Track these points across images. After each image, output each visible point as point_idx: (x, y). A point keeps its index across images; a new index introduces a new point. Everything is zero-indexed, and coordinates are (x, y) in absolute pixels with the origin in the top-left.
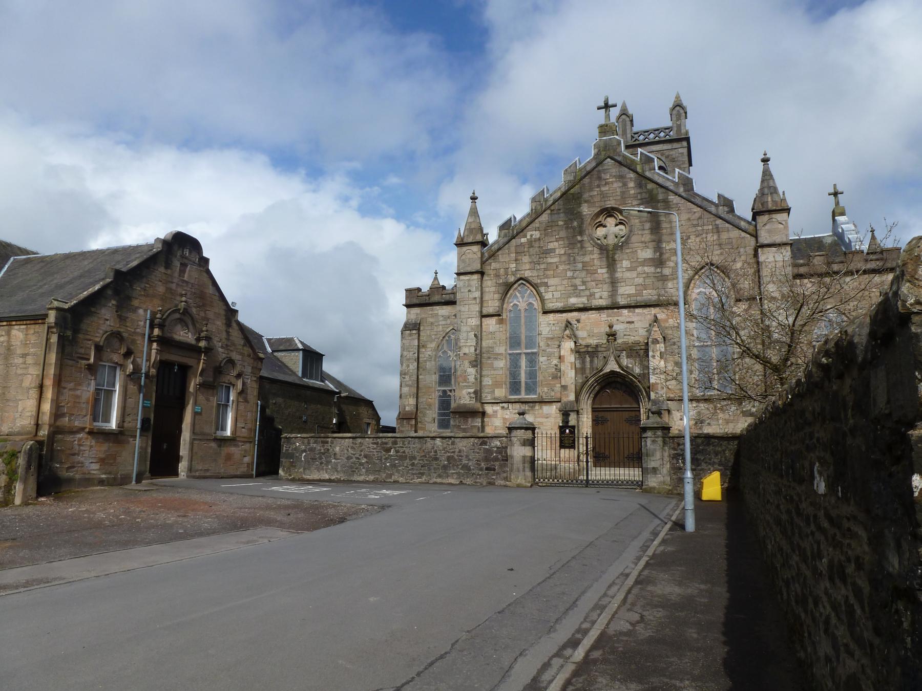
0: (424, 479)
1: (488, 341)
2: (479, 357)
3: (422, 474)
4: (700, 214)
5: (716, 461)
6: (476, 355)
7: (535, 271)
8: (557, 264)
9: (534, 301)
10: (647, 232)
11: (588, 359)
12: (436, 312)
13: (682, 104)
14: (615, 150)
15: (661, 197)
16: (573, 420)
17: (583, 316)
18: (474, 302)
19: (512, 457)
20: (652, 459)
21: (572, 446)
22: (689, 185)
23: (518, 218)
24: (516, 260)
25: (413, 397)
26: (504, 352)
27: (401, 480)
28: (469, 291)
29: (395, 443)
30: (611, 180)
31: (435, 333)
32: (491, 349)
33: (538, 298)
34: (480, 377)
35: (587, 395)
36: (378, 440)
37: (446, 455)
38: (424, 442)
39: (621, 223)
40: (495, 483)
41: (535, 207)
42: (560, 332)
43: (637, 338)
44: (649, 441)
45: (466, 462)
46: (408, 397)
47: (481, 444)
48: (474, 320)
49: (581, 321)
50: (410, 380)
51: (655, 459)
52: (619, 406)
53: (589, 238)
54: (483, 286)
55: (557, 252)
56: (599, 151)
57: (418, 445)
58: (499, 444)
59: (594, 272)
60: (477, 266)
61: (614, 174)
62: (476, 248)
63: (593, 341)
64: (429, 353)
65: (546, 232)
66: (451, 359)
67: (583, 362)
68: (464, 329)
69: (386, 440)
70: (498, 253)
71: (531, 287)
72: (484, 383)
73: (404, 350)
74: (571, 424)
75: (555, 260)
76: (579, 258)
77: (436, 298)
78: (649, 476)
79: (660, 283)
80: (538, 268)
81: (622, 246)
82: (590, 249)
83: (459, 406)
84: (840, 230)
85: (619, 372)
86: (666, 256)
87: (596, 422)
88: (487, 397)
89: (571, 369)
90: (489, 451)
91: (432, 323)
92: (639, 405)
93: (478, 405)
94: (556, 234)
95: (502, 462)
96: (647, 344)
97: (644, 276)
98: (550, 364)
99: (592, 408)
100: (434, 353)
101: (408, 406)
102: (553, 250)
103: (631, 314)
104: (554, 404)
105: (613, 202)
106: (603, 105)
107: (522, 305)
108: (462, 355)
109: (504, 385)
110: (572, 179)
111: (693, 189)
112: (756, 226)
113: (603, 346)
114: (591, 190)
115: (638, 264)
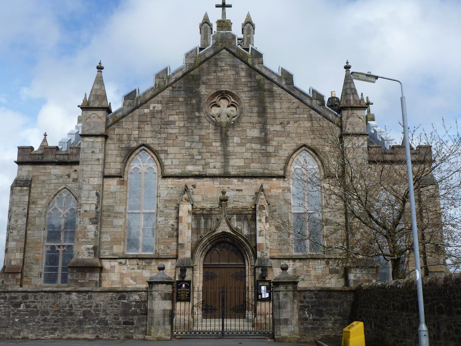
0: (56, 335)
1: (108, 200)
2: (100, 214)
3: (55, 330)
4: (297, 105)
5: (336, 312)
6: (97, 212)
7: (156, 139)
8: (177, 134)
9: (155, 166)
10: (254, 115)
11: (203, 221)
12: (49, 171)
13: (252, 22)
14: (230, 43)
15: (266, 87)
16: (189, 275)
17: (199, 182)
18: (97, 163)
19: (152, 311)
20: (284, 310)
21: (188, 299)
22: (290, 80)
23: (142, 92)
24: (139, 128)
25: (20, 252)
26: (124, 211)
27: (31, 336)
28: (93, 152)
29: (26, 297)
30: (226, 68)
31: (47, 191)
32: (111, 208)
33: (158, 164)
34: (99, 235)
35: (201, 253)
36: (7, 295)
37: (82, 310)
38: (59, 296)
39: (232, 105)
40: (132, 337)
41: (159, 83)
42: (177, 196)
43: (245, 204)
44: (281, 294)
45: (103, 316)
46: (15, 251)
47: (120, 299)
48: (96, 180)
49: (197, 187)
50: (18, 235)
51: (286, 310)
52: (227, 263)
53: (206, 115)
54: (106, 149)
55: (177, 124)
56: (217, 42)
57: (51, 300)
58: (137, 298)
59: (210, 144)
60: (102, 130)
61: (228, 63)
62: (101, 113)
63: (208, 205)
64: (40, 209)
65: (168, 105)
66: (62, 216)
67: (199, 223)
68: (86, 187)
69: (16, 295)
70: (121, 120)
71: (152, 154)
72: (103, 240)
73: (13, 206)
74: (187, 278)
76: (196, 131)
77: (50, 158)
78: (281, 326)
79: (265, 158)
80: (159, 136)
81: (233, 125)
82: (206, 124)
83: (77, 261)
84: (373, 132)
85: (230, 233)
86: (270, 136)
87: (206, 277)
88: (106, 253)
89: (188, 229)
90: (128, 306)
91: (44, 181)
92: (244, 262)
93: (97, 260)
94: (177, 108)
95: (141, 316)
96: (255, 209)
97: (252, 151)
98: (167, 223)
99: (204, 265)
100: (44, 210)
101: (14, 260)
102: (173, 122)
103: (240, 183)
104: (169, 260)
105: (227, 86)
106: (221, 3)
107: (143, 169)
108: (83, 212)
109: (122, 242)
110: (192, 62)
111: (293, 84)
112: (341, 118)
113: (216, 209)
114: (208, 74)
115: (247, 141)
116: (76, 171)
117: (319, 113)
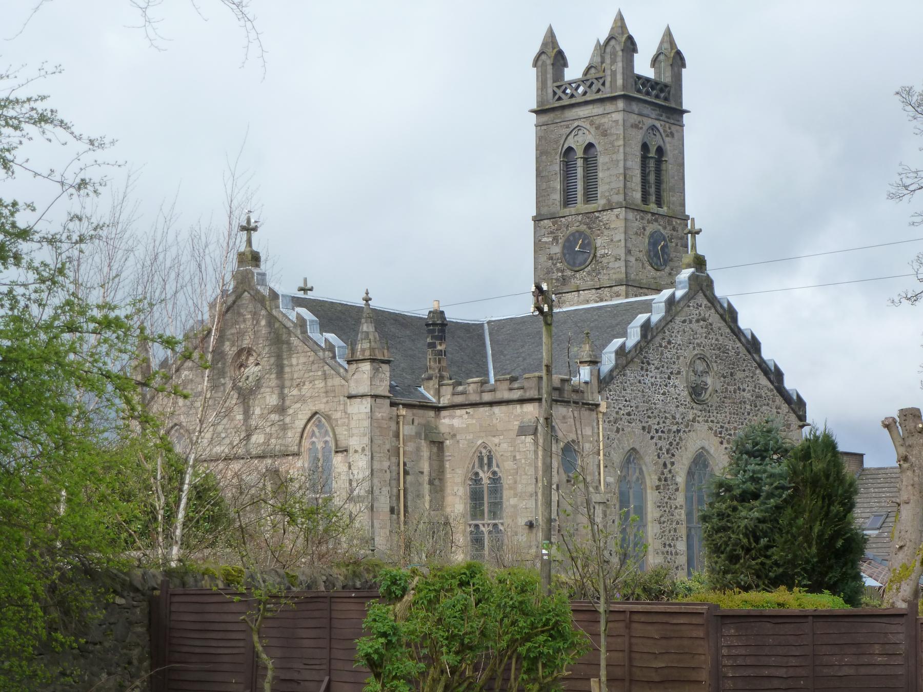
86: (287, 403)
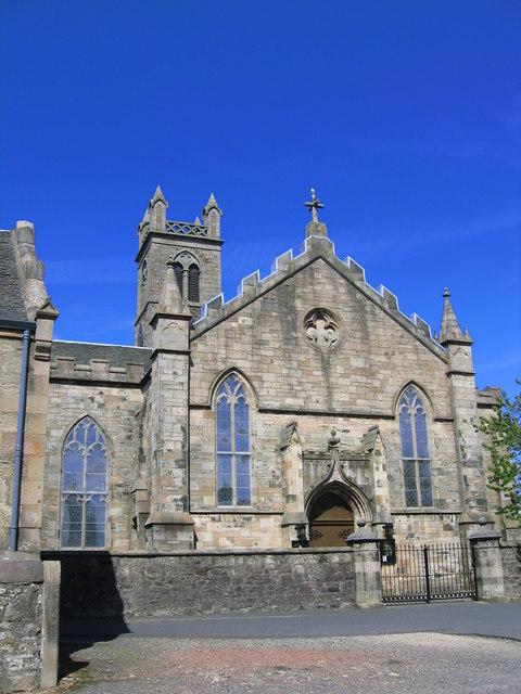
28: (175, 373)
34: (188, 481)
39: (330, 327)
60: (185, 347)
68: (168, 419)
75: (270, 353)
88: (195, 507)
91: (58, 405)
114: (304, 286)
116: (101, 393)
117: (424, 345)
